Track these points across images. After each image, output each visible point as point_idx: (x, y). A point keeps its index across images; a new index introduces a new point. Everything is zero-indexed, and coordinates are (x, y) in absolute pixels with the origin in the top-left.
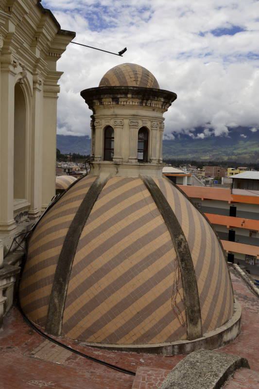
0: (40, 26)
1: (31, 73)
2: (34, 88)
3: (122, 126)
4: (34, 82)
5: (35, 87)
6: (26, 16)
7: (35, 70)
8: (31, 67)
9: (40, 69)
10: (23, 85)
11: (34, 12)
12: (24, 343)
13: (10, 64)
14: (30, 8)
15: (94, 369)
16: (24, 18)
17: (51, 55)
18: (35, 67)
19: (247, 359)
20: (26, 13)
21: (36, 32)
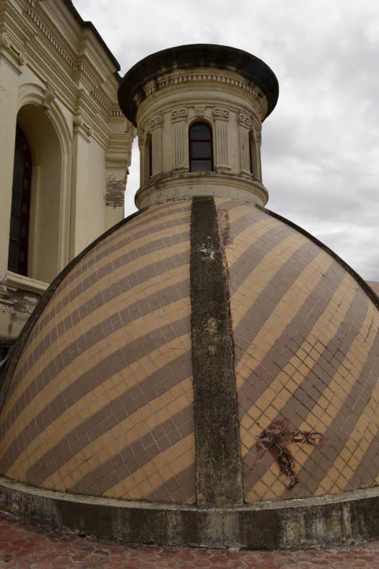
0: (81, 47)
1: (72, 113)
2: (74, 132)
3: (184, 117)
4: (75, 125)
5: (76, 130)
6: (102, 85)
7: (76, 110)
8: (72, 103)
9: (84, 107)
10: (49, 111)
11: (111, 82)
12: (13, 311)
13: (80, 125)
14: (108, 78)
15: (312, 494)
16: (99, 86)
17: (115, 113)
18: (77, 103)
19: (189, 122)
20: (103, 81)
21: (77, 57)
